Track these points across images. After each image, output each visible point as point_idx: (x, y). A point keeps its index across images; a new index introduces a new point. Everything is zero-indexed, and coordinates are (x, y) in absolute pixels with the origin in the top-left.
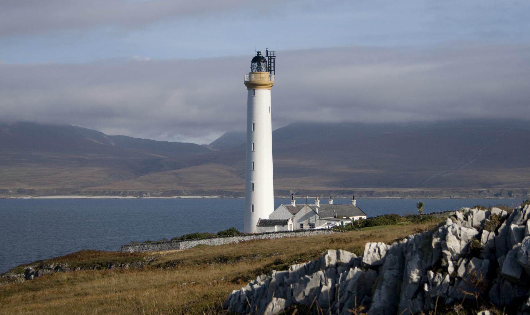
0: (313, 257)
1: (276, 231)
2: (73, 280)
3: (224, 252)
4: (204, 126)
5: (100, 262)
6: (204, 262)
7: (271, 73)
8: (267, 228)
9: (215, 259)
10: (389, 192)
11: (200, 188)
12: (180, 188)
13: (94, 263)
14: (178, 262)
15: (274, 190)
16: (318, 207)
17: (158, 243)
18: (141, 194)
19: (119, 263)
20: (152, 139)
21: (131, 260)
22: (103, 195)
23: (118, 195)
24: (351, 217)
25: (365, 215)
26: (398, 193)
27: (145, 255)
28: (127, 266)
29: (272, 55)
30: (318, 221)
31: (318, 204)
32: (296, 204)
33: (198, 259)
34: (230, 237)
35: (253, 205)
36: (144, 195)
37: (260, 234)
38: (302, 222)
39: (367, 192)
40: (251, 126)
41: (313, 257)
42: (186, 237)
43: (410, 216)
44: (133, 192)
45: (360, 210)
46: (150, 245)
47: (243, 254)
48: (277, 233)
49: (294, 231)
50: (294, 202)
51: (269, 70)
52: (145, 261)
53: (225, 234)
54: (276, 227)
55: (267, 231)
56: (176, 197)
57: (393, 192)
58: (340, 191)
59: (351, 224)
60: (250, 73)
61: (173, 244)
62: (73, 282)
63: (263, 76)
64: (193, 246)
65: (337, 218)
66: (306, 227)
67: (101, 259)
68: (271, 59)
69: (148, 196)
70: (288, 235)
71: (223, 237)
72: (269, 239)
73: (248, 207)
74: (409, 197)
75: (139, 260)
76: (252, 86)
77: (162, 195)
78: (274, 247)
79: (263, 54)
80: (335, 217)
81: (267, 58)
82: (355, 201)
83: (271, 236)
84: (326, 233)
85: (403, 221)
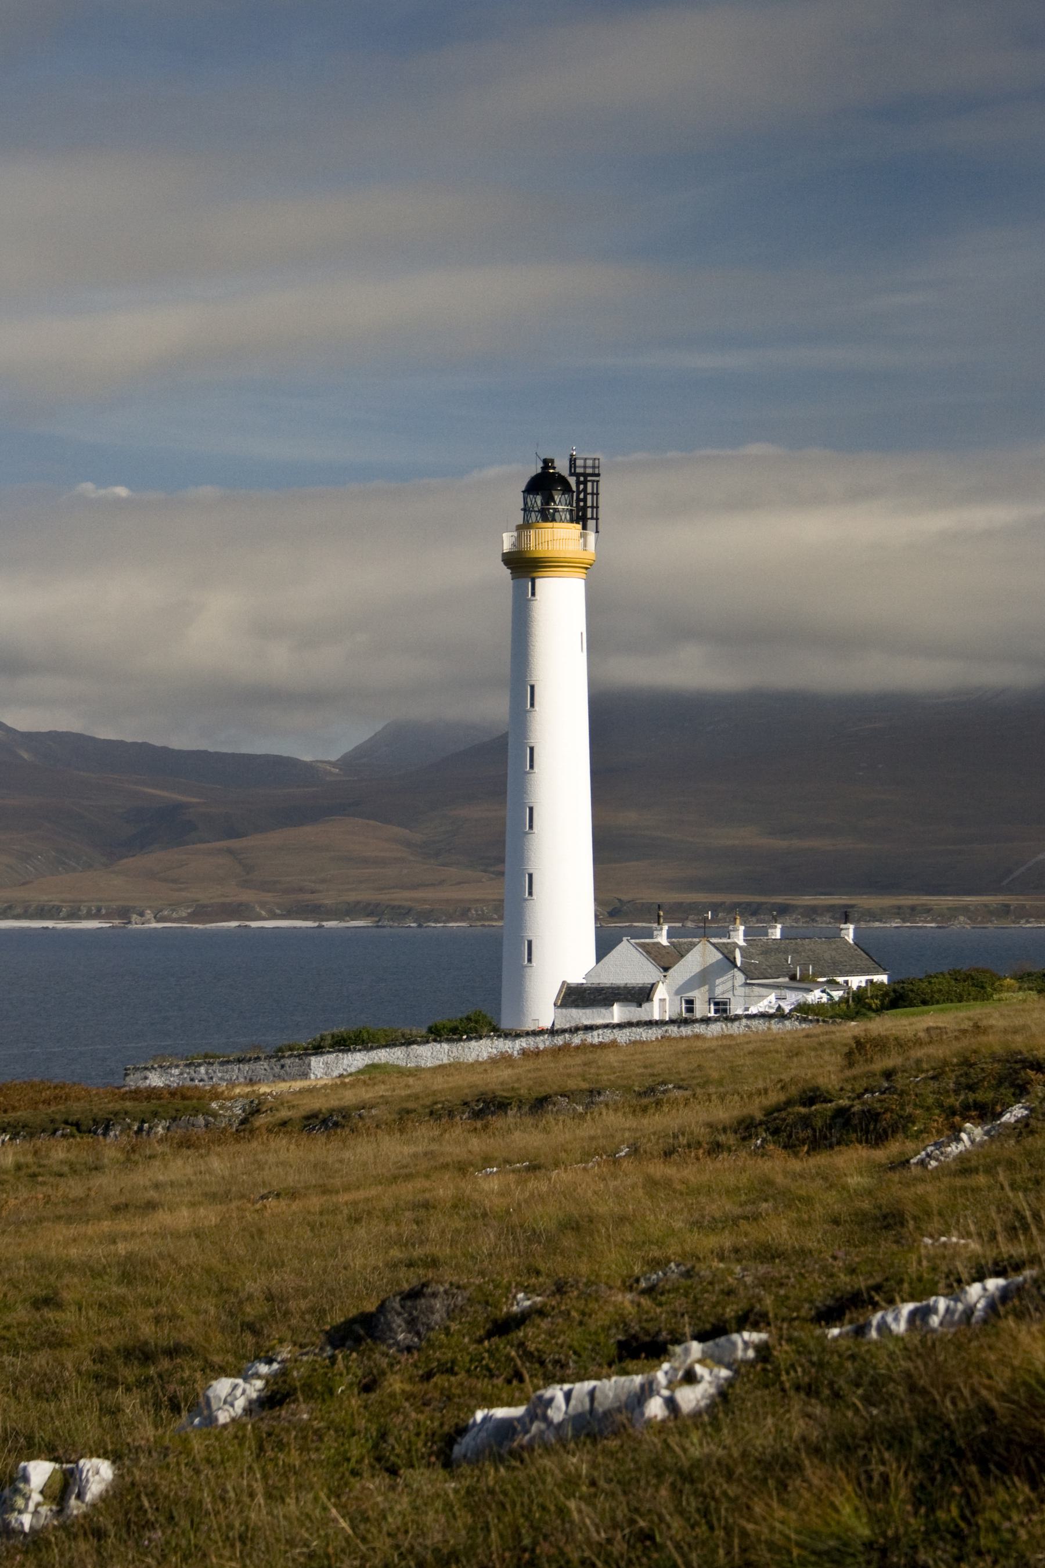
0: (933, 1078)
1: (616, 1021)
2: (34, 1169)
3: (499, 1079)
4: (314, 698)
5: (72, 1118)
6: (431, 1113)
7: (584, 528)
8: (588, 1011)
9: (466, 1104)
10: (899, 907)
11: (308, 896)
12: (247, 896)
13: (52, 1121)
14: (345, 1113)
15: (595, 900)
16: (740, 948)
17: (240, 1061)
18: (124, 913)
19: (134, 1119)
20: (158, 742)
21: (174, 1113)
22: (7, 918)
23: (51, 918)
24: (840, 980)
25: (884, 970)
26: (929, 911)
27: (216, 1096)
28: (160, 1130)
29: (589, 471)
30: (740, 991)
31: (739, 937)
32: (669, 936)
33: (410, 1105)
34: (469, 1039)
35: (530, 943)
36: (134, 917)
37: (563, 1031)
38: (690, 995)
39: (831, 908)
40: (522, 693)
41: (933, 1078)
42: (329, 1041)
43: (1030, 974)
44: (99, 910)
45: (870, 954)
46: (216, 1067)
47: (555, 1088)
48: (620, 1026)
49: (672, 1022)
50: (664, 932)
51: (580, 517)
52: (215, 1115)
53: (454, 1030)
54: (616, 1007)
55: (587, 1022)
56: (234, 924)
57: (913, 908)
58: (749, 904)
59: (847, 1001)
60: (519, 528)
61: (288, 1062)
62: (34, 1175)
63: (561, 538)
64: (353, 1070)
65: (800, 981)
66: (703, 1009)
67: (77, 1109)
68: (585, 483)
69: (148, 921)
70: (653, 1034)
71: (449, 1041)
72: (614, 1043)
73: (498, 951)
74: (961, 924)
75: (196, 1111)
76: (525, 566)
77: (192, 918)
78: (652, 1066)
79: (562, 467)
80: (793, 978)
81: (572, 481)
82: (851, 927)
83: (594, 1037)
84: (775, 1026)
85: (1009, 989)
